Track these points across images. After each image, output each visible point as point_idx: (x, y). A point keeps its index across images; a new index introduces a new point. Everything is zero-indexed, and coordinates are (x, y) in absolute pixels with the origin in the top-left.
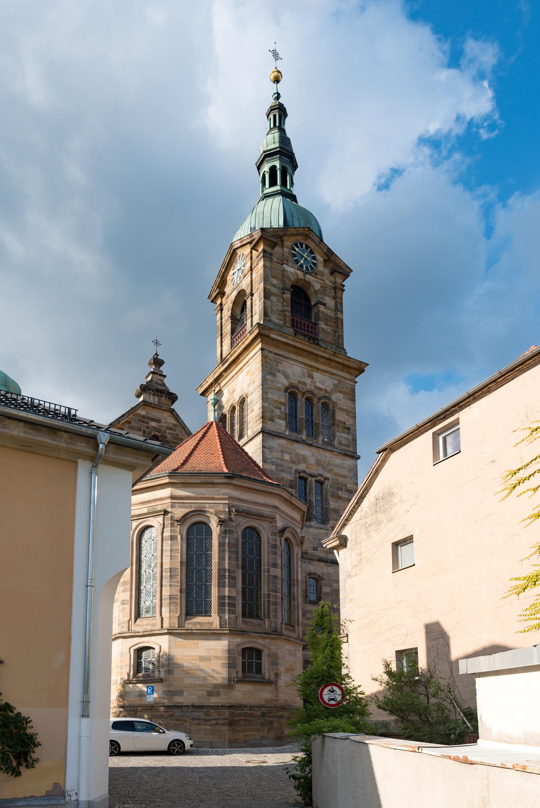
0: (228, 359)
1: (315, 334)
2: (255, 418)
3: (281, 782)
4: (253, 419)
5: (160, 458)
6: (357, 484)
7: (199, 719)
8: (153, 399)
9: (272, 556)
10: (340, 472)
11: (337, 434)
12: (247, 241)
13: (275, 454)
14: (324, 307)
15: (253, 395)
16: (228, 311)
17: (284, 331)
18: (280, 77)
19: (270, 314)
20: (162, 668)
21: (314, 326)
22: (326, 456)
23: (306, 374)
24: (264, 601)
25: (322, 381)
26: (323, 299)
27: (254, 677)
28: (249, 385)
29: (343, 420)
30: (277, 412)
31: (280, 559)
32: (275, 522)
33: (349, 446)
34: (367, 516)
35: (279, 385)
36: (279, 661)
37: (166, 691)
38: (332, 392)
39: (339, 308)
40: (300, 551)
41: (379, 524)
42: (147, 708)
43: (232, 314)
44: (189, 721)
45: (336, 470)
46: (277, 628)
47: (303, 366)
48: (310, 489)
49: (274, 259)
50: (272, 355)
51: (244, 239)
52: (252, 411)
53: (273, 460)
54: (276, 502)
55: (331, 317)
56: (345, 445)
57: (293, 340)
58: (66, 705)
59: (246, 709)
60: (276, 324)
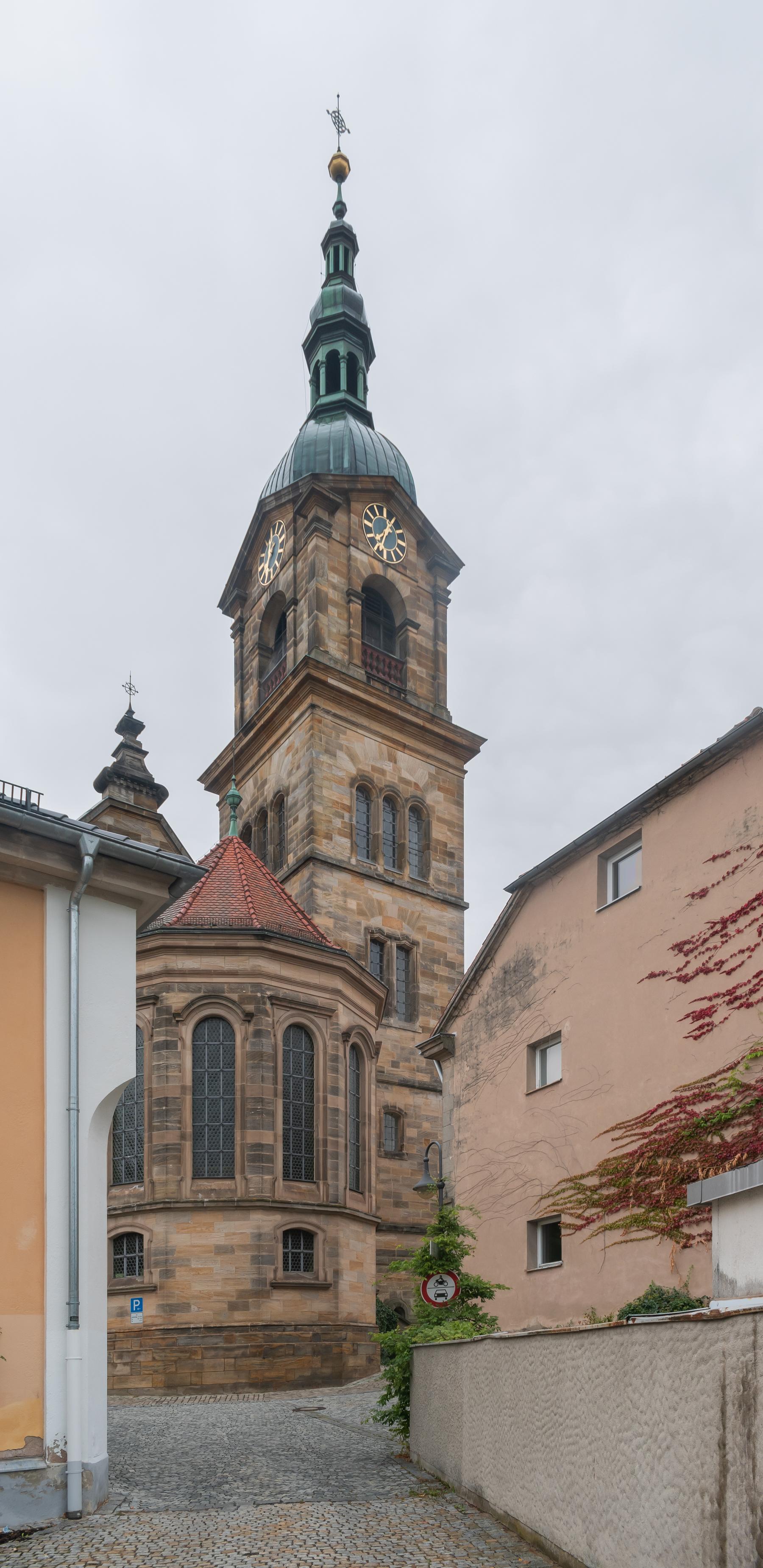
0: (255, 724)
1: (401, 682)
2: (301, 832)
3: (353, 1434)
4: (297, 835)
5: (184, 884)
6: (462, 953)
7: (216, 1349)
8: (125, 796)
9: (330, 1075)
10: (437, 932)
11: (434, 864)
12: (287, 498)
13: (334, 898)
14: (415, 631)
15: (298, 791)
16: (254, 632)
17: (351, 673)
18: (347, 170)
19: (327, 641)
20: (156, 1267)
21: (399, 666)
22: (415, 904)
23: (386, 755)
24: (318, 1151)
25: (410, 769)
26: (416, 616)
27: (302, 1277)
28: (290, 774)
29: (444, 840)
30: (338, 823)
31: (344, 1080)
32: (337, 1016)
33: (451, 885)
34: (490, 1000)
35: (341, 774)
36: (340, 1251)
37: (163, 1305)
38: (426, 789)
39: (439, 635)
40: (374, 1067)
41: (508, 1014)
42: (133, 1334)
43: (260, 637)
44: (200, 1352)
45: (430, 928)
46: (337, 1195)
47: (380, 740)
48: (388, 961)
49: (336, 535)
50: (330, 718)
51: (283, 493)
52: (296, 820)
53: (331, 910)
54: (338, 983)
55: (427, 650)
56: (445, 884)
57: (366, 691)
58: (42, 1310)
59: (288, 1328)
60: (336, 661)
